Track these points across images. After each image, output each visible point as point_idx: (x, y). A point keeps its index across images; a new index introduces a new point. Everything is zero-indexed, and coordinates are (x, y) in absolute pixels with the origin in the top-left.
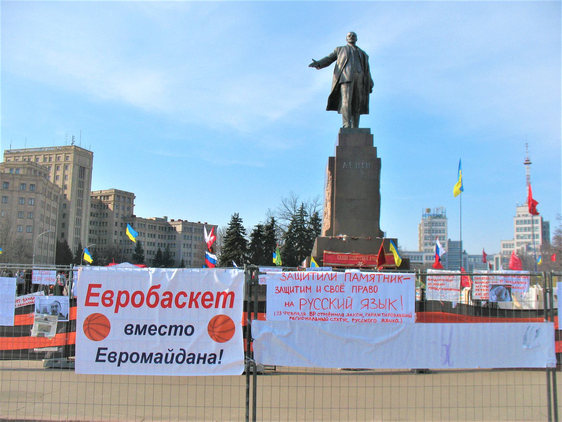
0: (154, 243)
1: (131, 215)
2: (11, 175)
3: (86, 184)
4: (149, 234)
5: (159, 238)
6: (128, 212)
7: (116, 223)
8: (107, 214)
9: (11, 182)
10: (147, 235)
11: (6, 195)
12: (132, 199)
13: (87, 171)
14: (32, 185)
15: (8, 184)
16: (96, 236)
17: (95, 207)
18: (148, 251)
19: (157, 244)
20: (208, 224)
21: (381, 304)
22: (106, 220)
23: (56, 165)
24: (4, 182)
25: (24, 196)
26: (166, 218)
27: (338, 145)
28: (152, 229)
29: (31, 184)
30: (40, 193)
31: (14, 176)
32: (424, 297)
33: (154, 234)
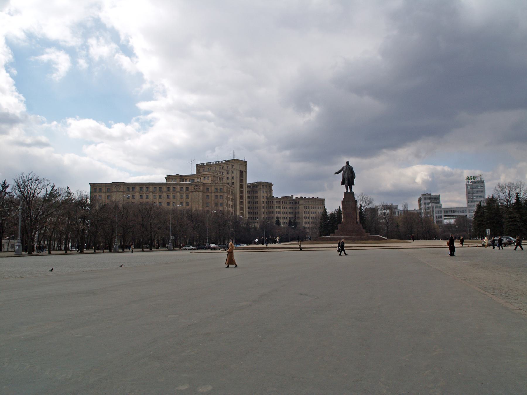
0: (286, 217)
1: (271, 196)
3: (244, 180)
4: (283, 207)
5: (289, 214)
6: (270, 195)
7: (263, 202)
8: (257, 197)
9: (210, 188)
10: (282, 208)
11: (208, 195)
12: (271, 187)
13: (244, 173)
14: (221, 188)
16: (251, 210)
17: (250, 193)
18: (283, 212)
19: (288, 218)
20: (319, 198)
21: (8, 250)
22: (256, 200)
23: (226, 171)
25: (217, 195)
26: (292, 196)
27: (352, 186)
28: (284, 203)
30: (225, 193)
33: (286, 207)
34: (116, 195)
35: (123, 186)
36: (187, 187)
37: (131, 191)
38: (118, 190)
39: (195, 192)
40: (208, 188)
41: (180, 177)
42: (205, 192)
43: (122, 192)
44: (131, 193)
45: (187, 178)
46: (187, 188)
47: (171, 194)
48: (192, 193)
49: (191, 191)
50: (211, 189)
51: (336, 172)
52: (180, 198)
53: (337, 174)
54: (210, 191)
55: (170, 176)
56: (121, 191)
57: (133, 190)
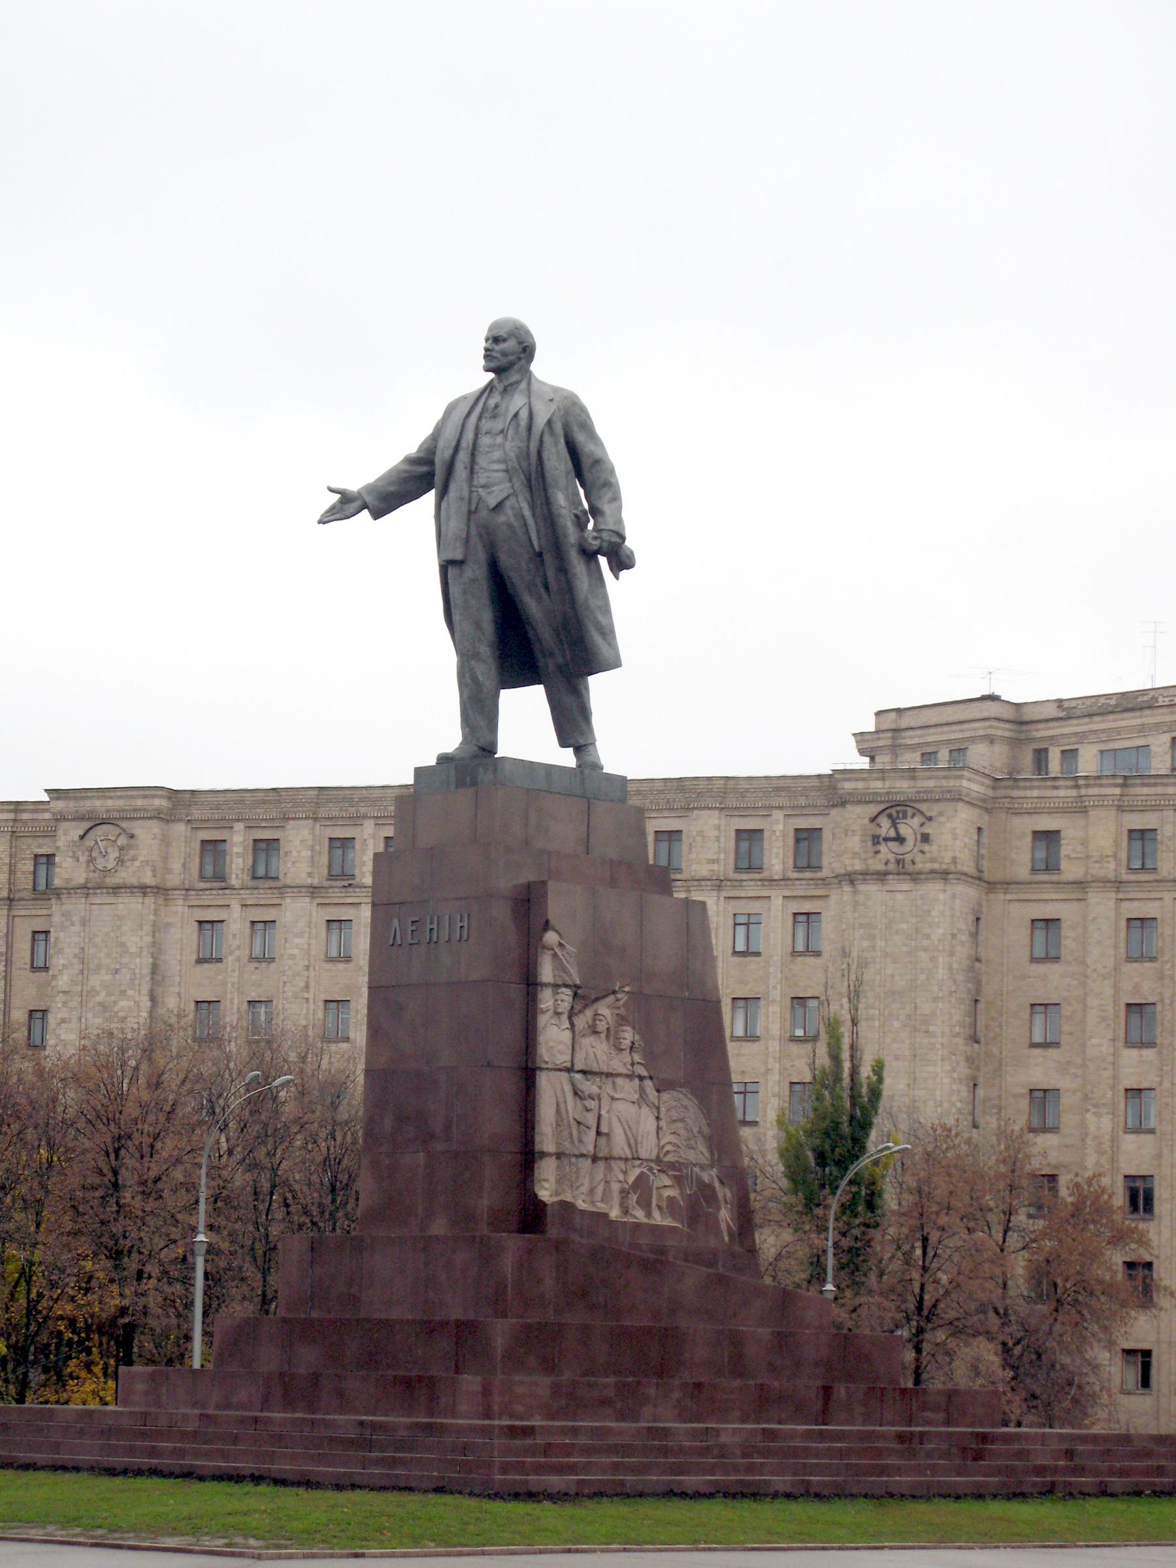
2: (1067, 787)
11: (1049, 911)
15: (1058, 841)
24: (1035, 833)
29: (1130, 831)
31: (1083, 792)
32: (425, 446)
34: (84, 923)
35: (155, 827)
36: (804, 823)
37: (234, 882)
38: (106, 872)
39: (881, 876)
40: (1048, 838)
41: (1003, 730)
42: (1008, 885)
43: (143, 889)
44: (236, 906)
45: (972, 739)
46: (806, 839)
47: (777, 902)
48: (847, 888)
49: (838, 868)
50: (1084, 843)
51: (355, 484)
52: (318, 949)
53: (377, 514)
54: (1070, 870)
55: (905, 722)
56: (134, 881)
57: (261, 871)
